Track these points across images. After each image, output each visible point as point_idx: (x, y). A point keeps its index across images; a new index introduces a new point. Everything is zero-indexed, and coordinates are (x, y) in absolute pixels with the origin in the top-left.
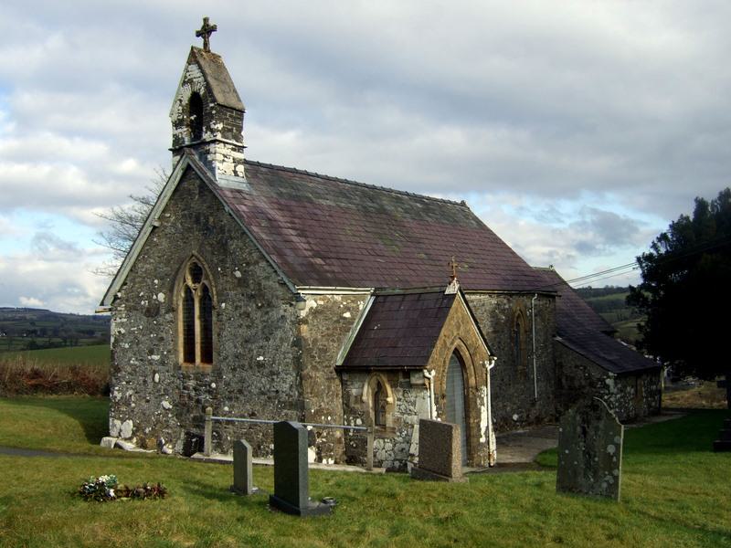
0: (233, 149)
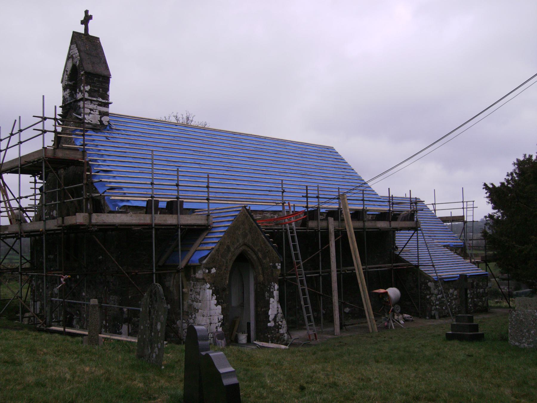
0: (99, 105)
